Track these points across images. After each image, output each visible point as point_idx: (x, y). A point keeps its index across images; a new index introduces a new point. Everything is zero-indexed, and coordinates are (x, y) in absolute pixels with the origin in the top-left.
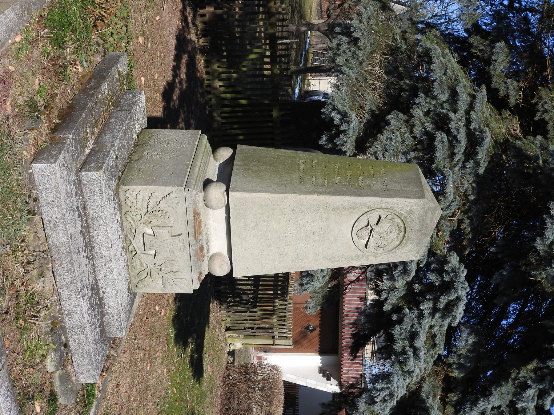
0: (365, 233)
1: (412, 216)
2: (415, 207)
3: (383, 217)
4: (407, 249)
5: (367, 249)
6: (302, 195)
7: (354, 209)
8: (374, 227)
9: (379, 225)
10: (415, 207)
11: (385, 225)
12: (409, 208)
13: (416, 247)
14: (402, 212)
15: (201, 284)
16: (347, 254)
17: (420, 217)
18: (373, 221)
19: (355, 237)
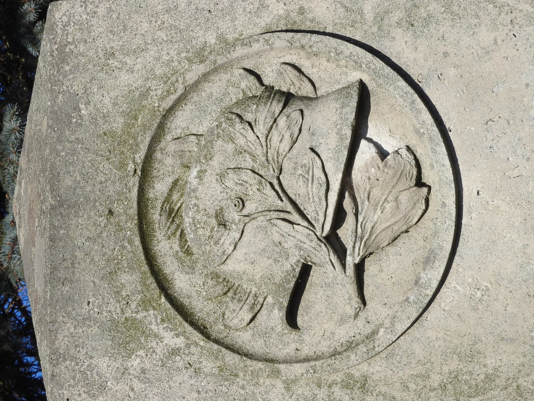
0: (379, 209)
1: (114, 307)
2: (103, 364)
3: (274, 317)
4: (124, 77)
5: (355, 76)
6: (195, 332)
7: (455, 378)
8: (323, 255)
9: (290, 265)
10: (103, 364)
11: (259, 255)
12: (135, 363)
13: (78, 88)
14: (171, 340)
15: (353, 131)
16: (485, 36)
17: (69, 299)
18: (330, 282)
19: (438, 172)
